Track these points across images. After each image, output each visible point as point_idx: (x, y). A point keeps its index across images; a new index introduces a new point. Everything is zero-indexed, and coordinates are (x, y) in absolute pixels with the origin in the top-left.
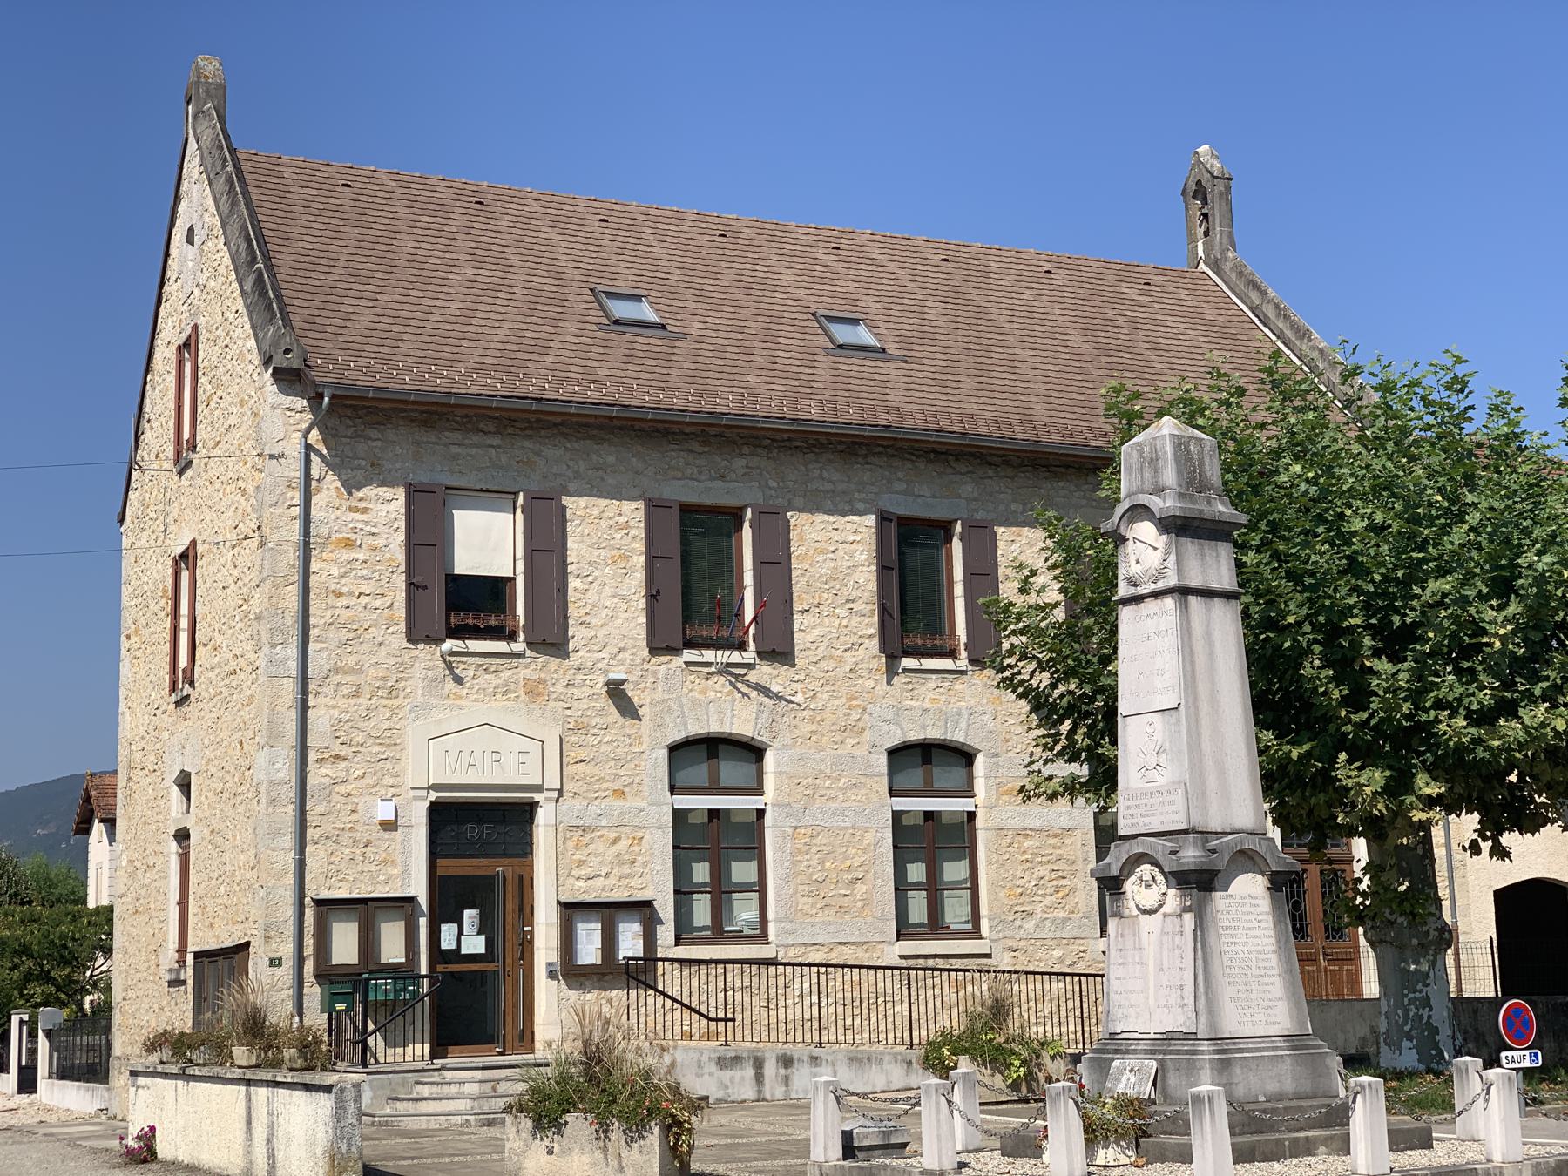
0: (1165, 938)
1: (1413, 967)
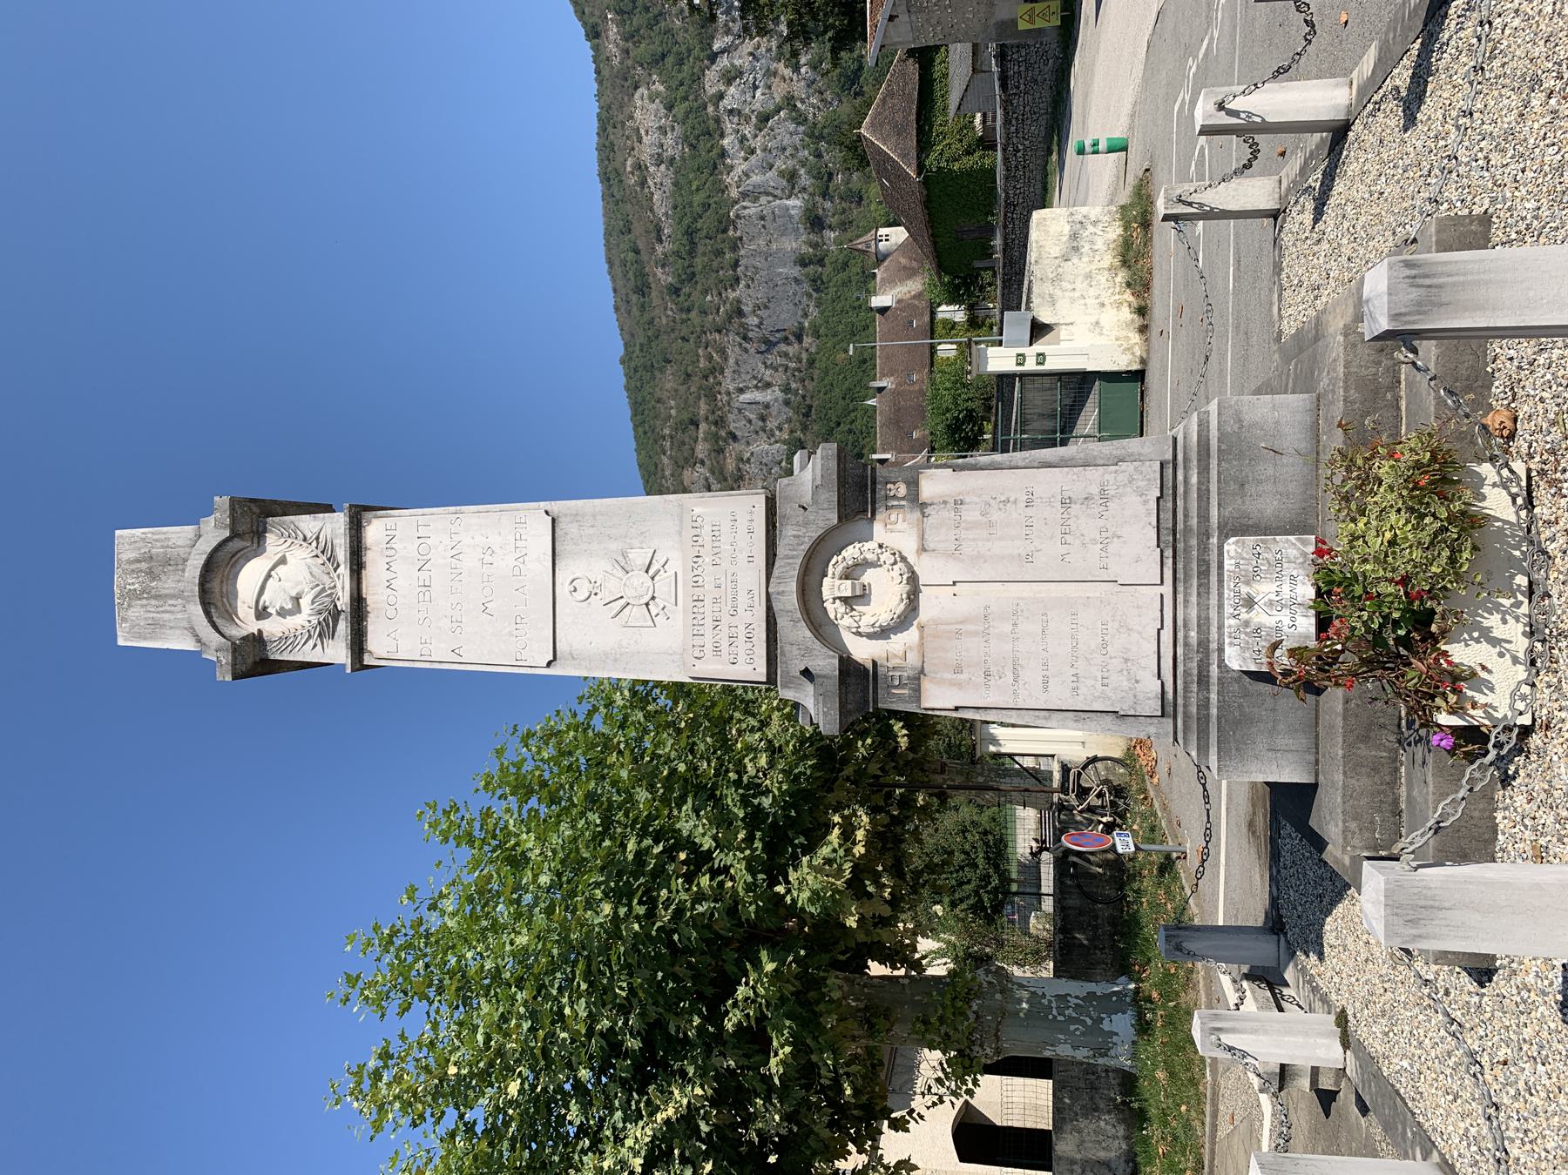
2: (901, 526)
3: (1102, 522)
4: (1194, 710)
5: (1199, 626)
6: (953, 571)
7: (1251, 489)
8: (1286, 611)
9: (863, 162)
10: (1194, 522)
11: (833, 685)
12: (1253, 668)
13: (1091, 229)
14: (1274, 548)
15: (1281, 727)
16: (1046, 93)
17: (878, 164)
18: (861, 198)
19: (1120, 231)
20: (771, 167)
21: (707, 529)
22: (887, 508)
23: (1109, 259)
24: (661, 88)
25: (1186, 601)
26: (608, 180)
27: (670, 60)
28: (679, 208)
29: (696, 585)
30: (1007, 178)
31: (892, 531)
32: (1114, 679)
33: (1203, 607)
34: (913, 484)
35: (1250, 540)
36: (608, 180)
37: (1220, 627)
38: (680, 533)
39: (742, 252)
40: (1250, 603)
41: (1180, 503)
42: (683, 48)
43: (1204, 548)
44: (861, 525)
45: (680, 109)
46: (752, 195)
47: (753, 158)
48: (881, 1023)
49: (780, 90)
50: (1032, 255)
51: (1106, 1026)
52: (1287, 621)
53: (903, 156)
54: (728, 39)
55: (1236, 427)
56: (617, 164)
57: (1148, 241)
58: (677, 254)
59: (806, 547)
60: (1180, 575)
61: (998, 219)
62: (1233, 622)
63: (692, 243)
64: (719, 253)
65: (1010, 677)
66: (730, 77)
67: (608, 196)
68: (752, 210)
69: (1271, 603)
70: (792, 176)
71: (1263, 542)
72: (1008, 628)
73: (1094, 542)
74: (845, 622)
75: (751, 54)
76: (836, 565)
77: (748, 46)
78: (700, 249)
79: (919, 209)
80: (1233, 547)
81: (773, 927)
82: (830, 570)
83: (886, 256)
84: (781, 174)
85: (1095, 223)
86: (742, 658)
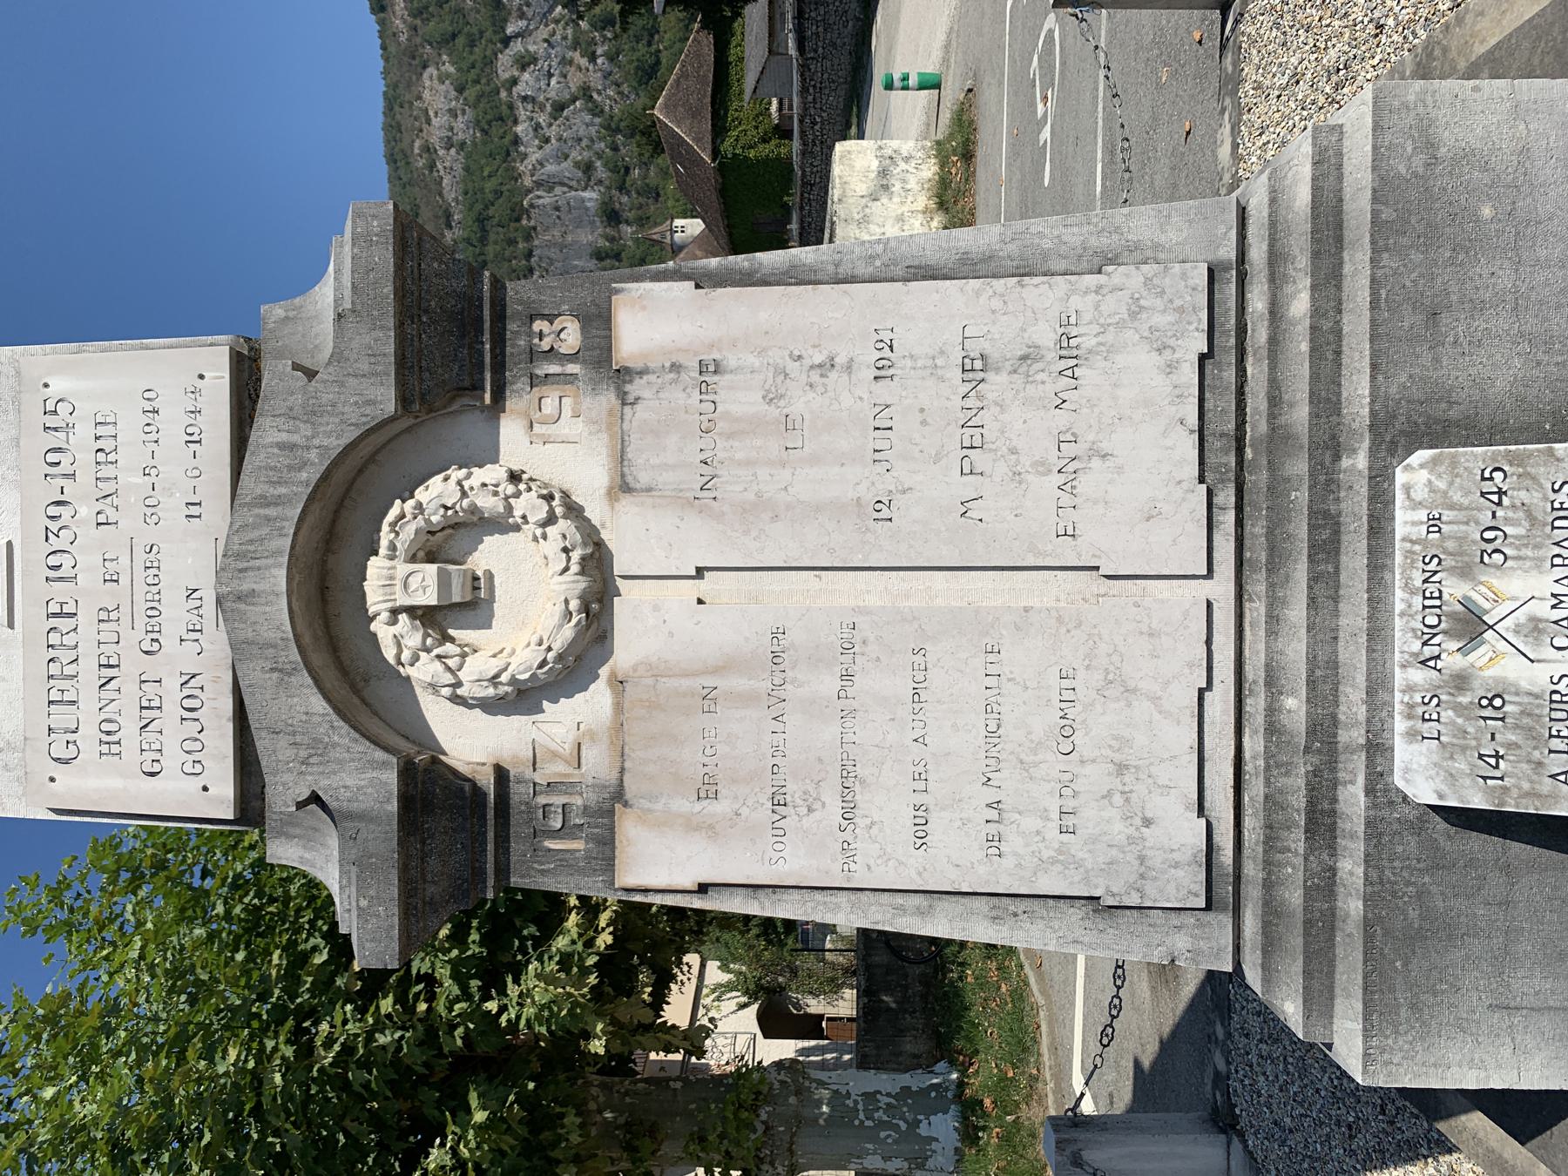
0: (732, 486)
1: (825, 1109)
2: (569, 426)
3: (1061, 419)
4: (1294, 897)
5: (1311, 683)
6: (701, 542)
7: (1455, 325)
9: (658, 148)
10: (1300, 415)
11: (384, 839)
12: (1478, 802)
13: (903, 166)
15: (1524, 947)
16: (845, 59)
17: (672, 149)
18: (658, 195)
19: (936, 168)
20: (566, 157)
21: (83, 433)
22: (534, 381)
23: (923, 201)
24: (452, 69)
25: (1273, 620)
26: (395, 162)
27: (460, 41)
28: (470, 194)
29: (55, 574)
30: (803, 153)
31: (547, 440)
32: (1090, 817)
33: (1323, 633)
34: (598, 322)
35: (1475, 456)
36: (395, 162)
37: (1378, 686)
38: (17, 442)
39: (536, 242)
41: (1256, 370)
42: (475, 30)
43: (1325, 483)
44: (468, 426)
45: (471, 92)
46: (548, 185)
47: (548, 147)
48: (646, 1144)
49: (575, 80)
50: (835, 192)
51: (923, 1130)
53: (697, 140)
54: (522, 24)
55: (1418, 162)
56: (405, 144)
57: (969, 176)
58: (468, 241)
59: (311, 475)
60: (1257, 552)
61: (793, 199)
62: (1418, 675)
63: (483, 230)
64: (512, 242)
65: (833, 809)
66: (524, 62)
67: (394, 178)
68: (547, 200)
69: (1535, 628)
70: (588, 168)
71: (1514, 459)
72: (829, 684)
73: (1042, 467)
74: (424, 671)
75: (546, 40)
76: (401, 524)
77: (543, 33)
78: (492, 237)
79: (714, 197)
80: (1424, 475)
81: (493, 1057)
82: (385, 537)
83: (681, 248)
84: (577, 165)
85: (907, 159)
86: (173, 759)
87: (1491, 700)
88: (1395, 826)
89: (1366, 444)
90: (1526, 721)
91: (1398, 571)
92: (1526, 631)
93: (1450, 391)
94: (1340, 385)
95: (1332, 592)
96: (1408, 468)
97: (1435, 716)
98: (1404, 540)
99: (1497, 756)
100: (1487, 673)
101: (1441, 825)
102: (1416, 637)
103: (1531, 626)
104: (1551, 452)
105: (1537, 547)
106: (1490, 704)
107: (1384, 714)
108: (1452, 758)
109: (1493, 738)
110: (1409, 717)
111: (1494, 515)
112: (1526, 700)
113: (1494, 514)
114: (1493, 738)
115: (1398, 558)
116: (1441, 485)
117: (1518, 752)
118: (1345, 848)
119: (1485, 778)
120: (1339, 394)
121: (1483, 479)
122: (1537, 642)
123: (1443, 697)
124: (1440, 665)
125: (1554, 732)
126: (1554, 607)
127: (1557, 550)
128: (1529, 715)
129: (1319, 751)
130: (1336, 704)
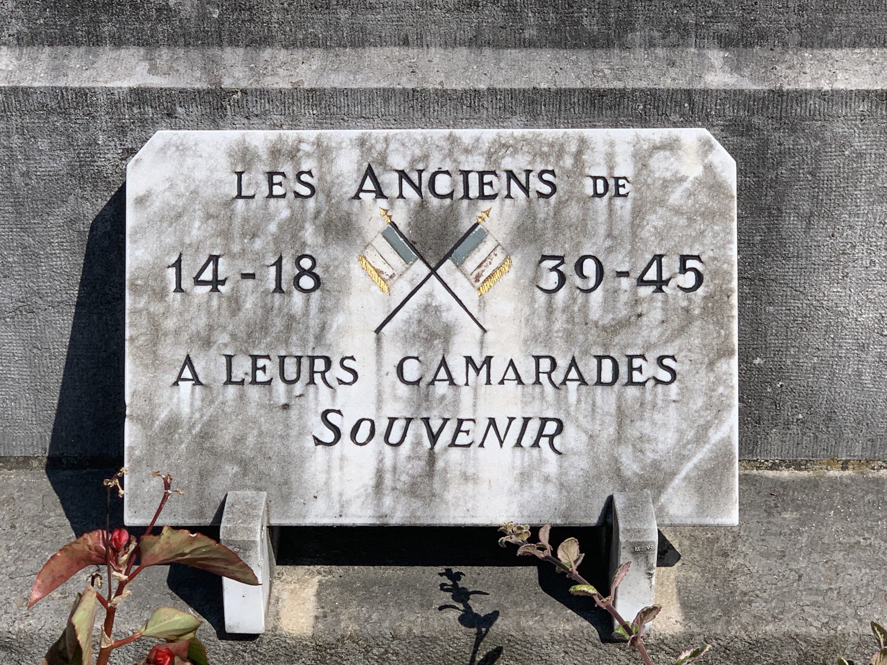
8: (398, 402)
12: (138, 255)
14: (687, 351)
19: (718, 365)
40: (435, 242)
52: (354, 403)
62: (347, 166)
69: (433, 333)
71: (714, 307)
80: (693, 170)
87: (310, 272)
88: (81, 137)
89: (748, 85)
90: (278, 323)
91: (528, 132)
92: (428, 320)
93: (829, 216)
94: (854, 45)
95: (488, 35)
96: (707, 147)
97: (277, 190)
98: (583, 141)
99: (216, 283)
100: (356, 269)
101: (92, 208)
102: (414, 161)
103: (438, 328)
104: (724, 353)
105: (569, 336)
106: (303, 272)
107: (277, 118)
108: (209, 216)
109: (245, 276)
110: (275, 153)
111: (621, 274)
112: (314, 322)
113: (626, 274)
114: (245, 276)
115: (549, 134)
116: (676, 197)
117: (225, 312)
118: (35, 60)
119: (178, 265)
120: (837, 44)
121: (684, 259)
122: (410, 338)
123: (311, 203)
124: (368, 198)
125: (261, 363)
126: (469, 360)
127: (563, 363)
128: (288, 328)
129: (203, 17)
130: (291, 44)
